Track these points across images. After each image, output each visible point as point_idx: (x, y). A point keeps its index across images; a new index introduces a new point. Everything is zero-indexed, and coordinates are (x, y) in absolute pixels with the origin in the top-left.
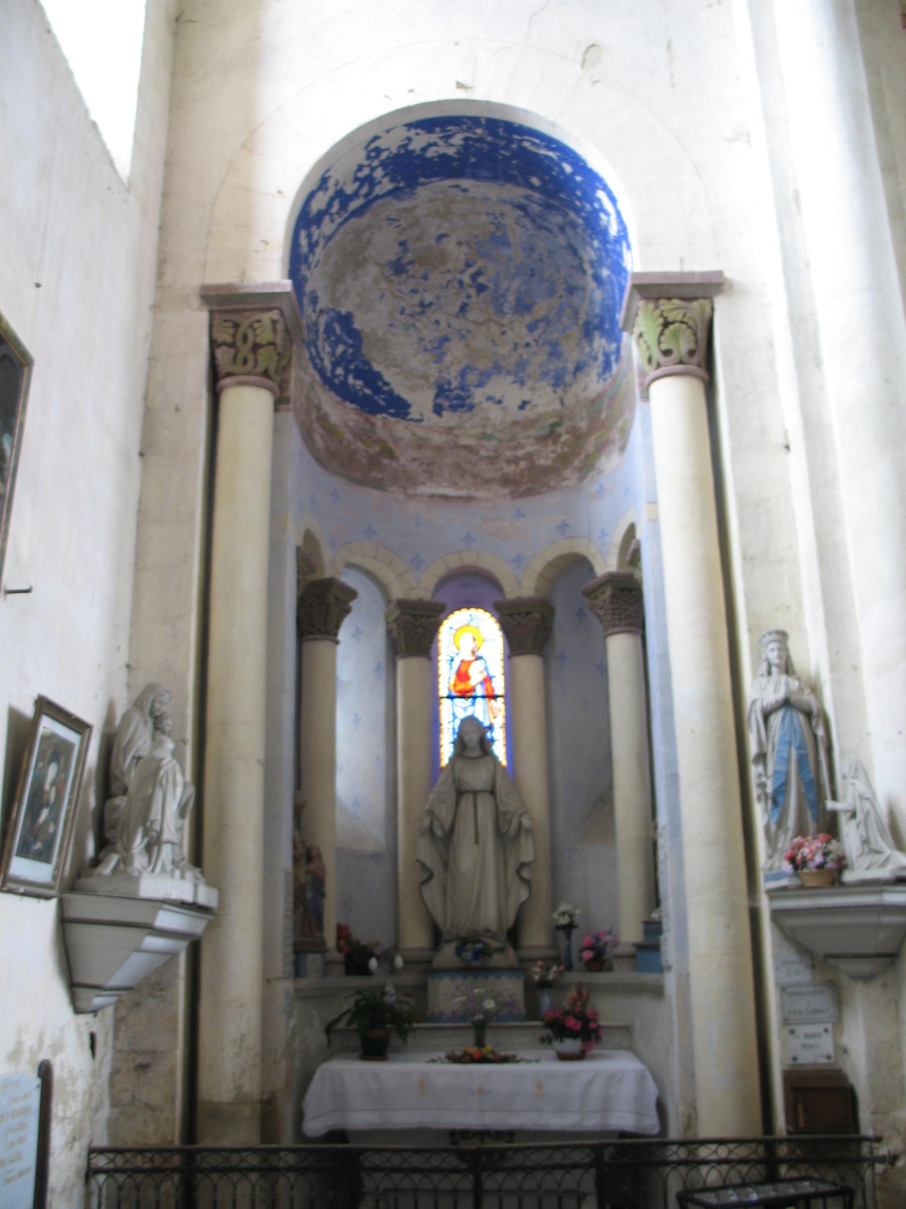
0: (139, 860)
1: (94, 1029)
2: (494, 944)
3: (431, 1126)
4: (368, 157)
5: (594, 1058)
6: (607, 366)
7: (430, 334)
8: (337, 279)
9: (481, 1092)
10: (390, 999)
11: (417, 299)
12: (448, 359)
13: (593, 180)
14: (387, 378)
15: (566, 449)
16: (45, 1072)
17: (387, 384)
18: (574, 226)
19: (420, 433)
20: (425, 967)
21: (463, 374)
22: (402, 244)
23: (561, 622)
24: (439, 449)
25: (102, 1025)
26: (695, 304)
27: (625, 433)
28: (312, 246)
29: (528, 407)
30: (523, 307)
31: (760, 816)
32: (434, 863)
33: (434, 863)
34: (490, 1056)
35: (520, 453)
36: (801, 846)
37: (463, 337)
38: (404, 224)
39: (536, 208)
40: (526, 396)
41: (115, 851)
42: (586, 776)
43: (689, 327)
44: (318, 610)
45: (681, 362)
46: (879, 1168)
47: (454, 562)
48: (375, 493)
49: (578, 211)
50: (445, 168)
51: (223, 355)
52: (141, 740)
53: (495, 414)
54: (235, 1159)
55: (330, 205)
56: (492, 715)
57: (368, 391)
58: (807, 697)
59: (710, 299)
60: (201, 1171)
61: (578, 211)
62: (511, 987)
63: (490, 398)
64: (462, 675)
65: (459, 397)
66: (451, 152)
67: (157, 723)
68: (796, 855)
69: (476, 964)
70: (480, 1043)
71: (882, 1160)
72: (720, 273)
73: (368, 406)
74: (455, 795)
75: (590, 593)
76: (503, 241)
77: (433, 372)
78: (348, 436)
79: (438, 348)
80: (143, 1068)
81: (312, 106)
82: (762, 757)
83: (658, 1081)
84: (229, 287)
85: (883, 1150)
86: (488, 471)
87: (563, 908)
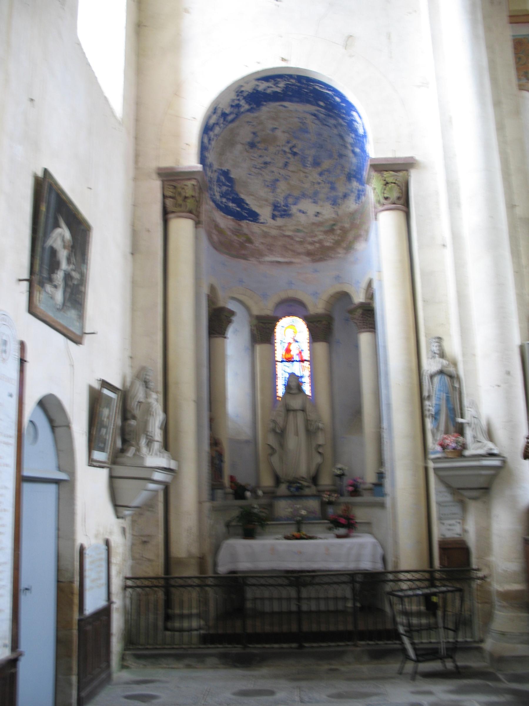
0: (144, 450)
1: (125, 526)
2: (305, 484)
3: (277, 569)
4: (238, 96)
5: (354, 537)
6: (359, 197)
7: (269, 178)
8: (221, 154)
9: (300, 553)
10: (256, 511)
11: (261, 160)
12: (279, 191)
13: (350, 107)
14: (248, 202)
15: (340, 238)
16: (107, 543)
17: (247, 204)
18: (341, 125)
19: (265, 229)
20: (272, 495)
21: (286, 198)
22: (254, 133)
23: (337, 325)
24: (274, 238)
25: (126, 523)
26: (401, 174)
27: (367, 232)
28: (210, 140)
29: (320, 216)
30: (316, 163)
31: (429, 424)
32: (275, 445)
33: (275, 445)
34: (305, 537)
35: (316, 239)
36: (445, 438)
37: (286, 179)
38: (255, 123)
39: (322, 116)
40: (318, 209)
41: (132, 445)
42: (348, 400)
43: (398, 186)
44: (217, 322)
45: (394, 204)
46: (479, 582)
47: (283, 295)
48: (243, 261)
49: (343, 119)
50: (275, 97)
51: (169, 202)
52: (140, 394)
53: (302, 219)
54: (190, 582)
55: (218, 120)
56: (303, 371)
57: (238, 209)
58: (451, 369)
59: (407, 170)
60: (174, 586)
61: (343, 119)
62: (314, 504)
63: (300, 211)
64: (288, 351)
65: (285, 211)
66: (278, 90)
67: (146, 383)
68: (348, 491)
69: (297, 493)
70: (299, 530)
71: (479, 578)
72: (412, 158)
73: (238, 217)
74: (287, 411)
75: (351, 312)
76: (305, 131)
77: (271, 197)
78: (229, 233)
79: (273, 185)
80: (145, 542)
81: (209, 71)
82: (429, 397)
83: (383, 547)
84: (171, 168)
85: (480, 574)
86: (300, 248)
87: (339, 466)
